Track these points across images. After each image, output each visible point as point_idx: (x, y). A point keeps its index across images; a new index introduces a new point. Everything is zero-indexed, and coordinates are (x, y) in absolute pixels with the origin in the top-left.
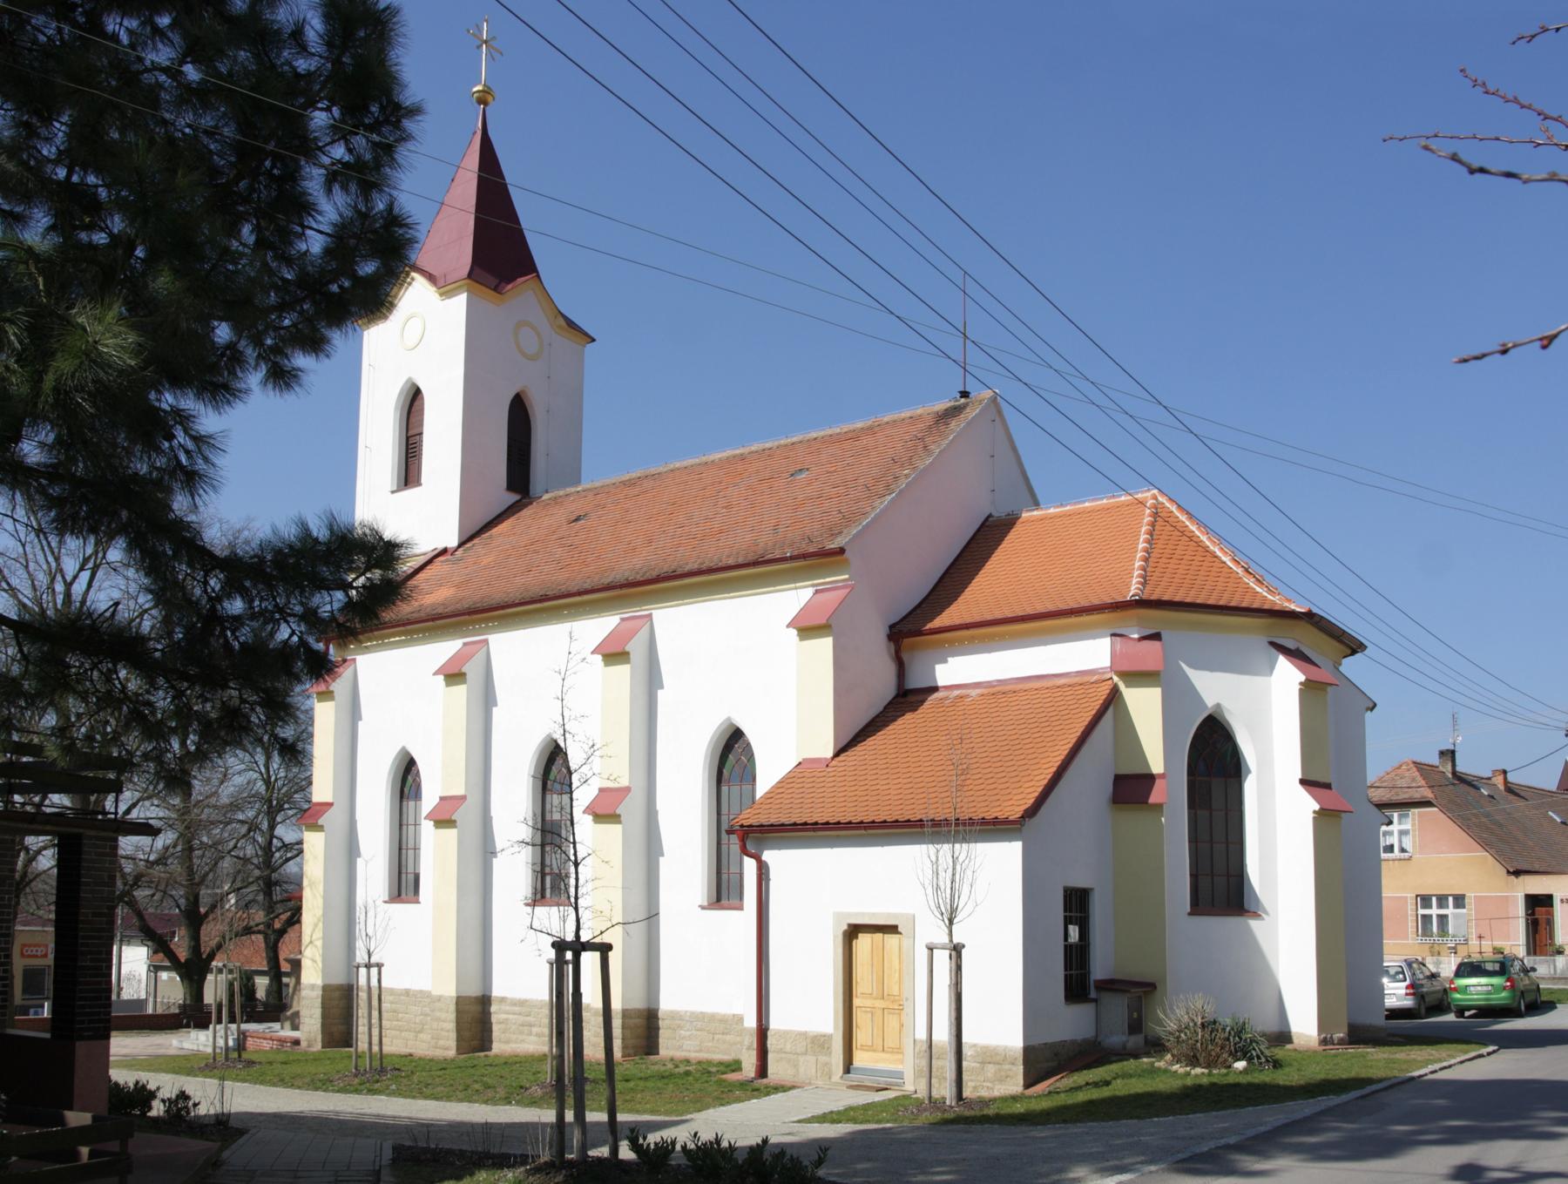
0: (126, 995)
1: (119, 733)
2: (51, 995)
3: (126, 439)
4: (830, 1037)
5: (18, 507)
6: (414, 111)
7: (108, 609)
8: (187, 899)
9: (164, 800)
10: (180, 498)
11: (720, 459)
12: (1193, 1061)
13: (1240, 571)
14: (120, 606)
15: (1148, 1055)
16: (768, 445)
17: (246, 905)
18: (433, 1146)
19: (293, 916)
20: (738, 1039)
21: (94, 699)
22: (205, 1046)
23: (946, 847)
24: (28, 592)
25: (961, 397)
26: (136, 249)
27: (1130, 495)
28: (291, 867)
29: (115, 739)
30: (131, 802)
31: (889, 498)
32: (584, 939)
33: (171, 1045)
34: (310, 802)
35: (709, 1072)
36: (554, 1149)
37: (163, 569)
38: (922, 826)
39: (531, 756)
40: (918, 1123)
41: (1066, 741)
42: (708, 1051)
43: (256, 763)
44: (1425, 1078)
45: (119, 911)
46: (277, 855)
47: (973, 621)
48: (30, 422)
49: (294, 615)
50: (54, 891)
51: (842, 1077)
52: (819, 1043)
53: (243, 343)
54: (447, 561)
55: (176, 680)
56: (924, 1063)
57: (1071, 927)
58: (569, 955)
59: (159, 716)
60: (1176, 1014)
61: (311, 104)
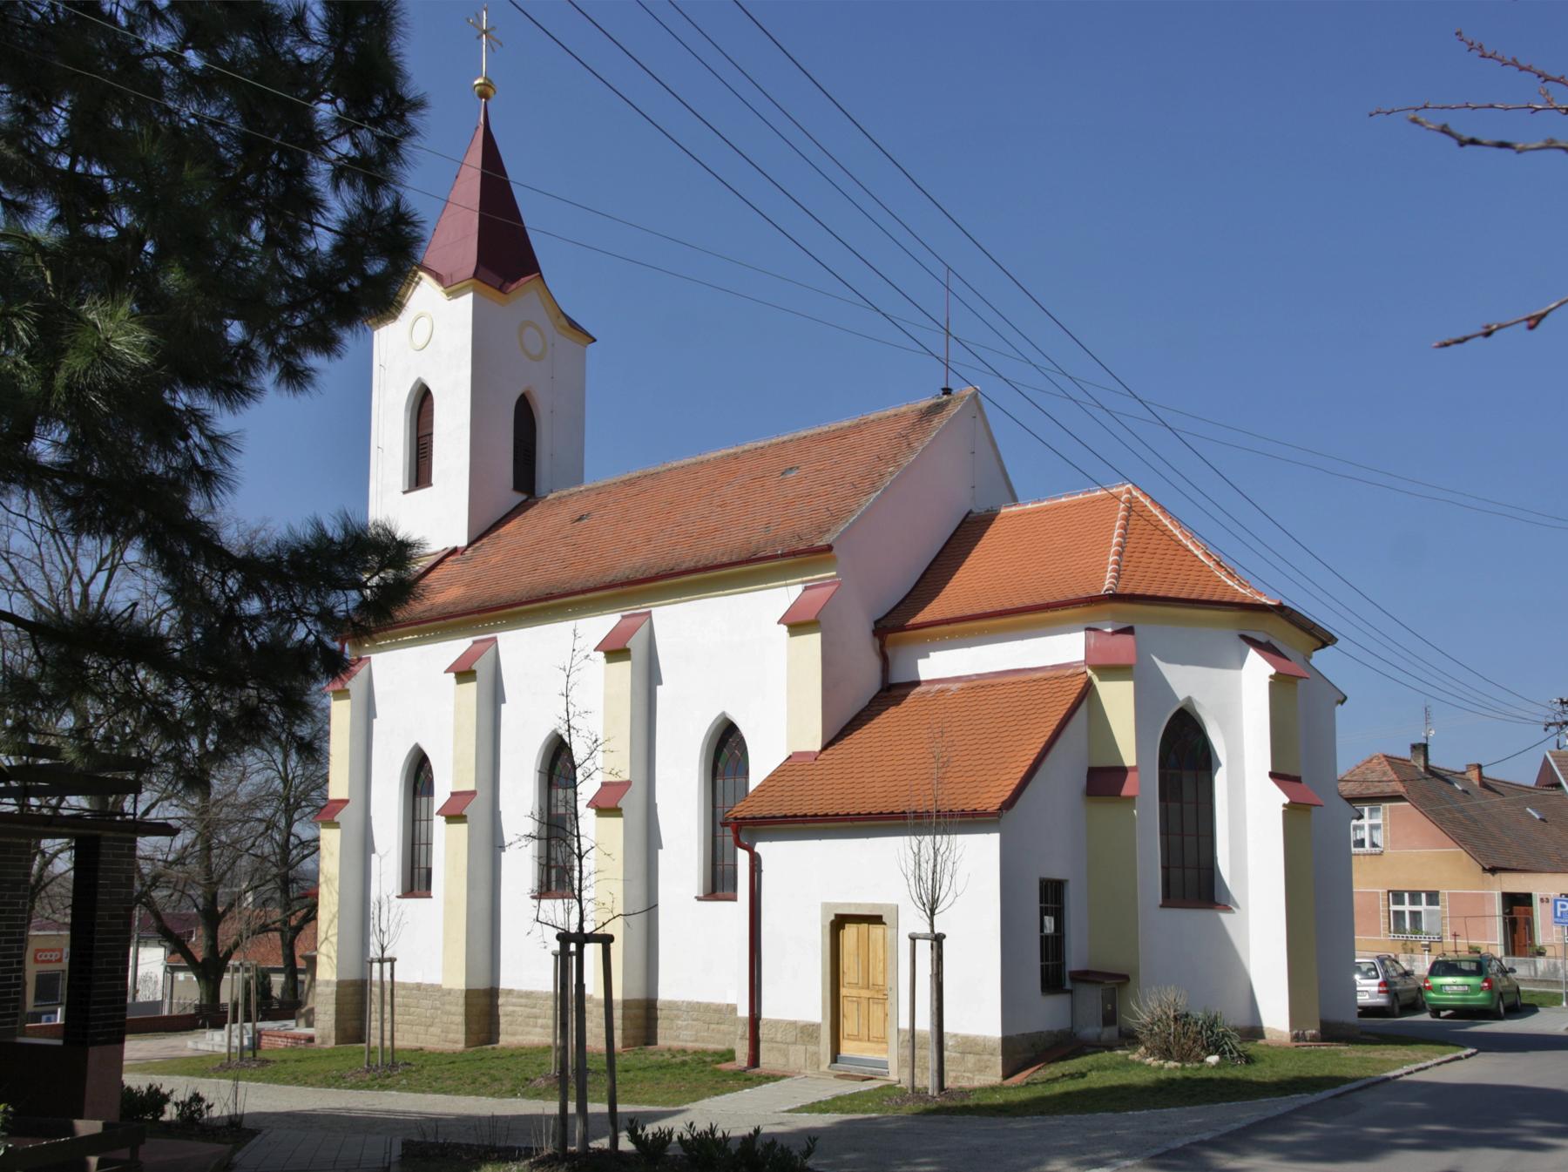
0: (142, 997)
1: (138, 734)
2: (65, 1001)
3: (141, 438)
4: (818, 1026)
5: (32, 507)
6: (418, 105)
7: (126, 610)
8: (205, 898)
9: (183, 800)
10: (197, 498)
11: (715, 458)
12: (1166, 1054)
13: (1212, 564)
14: (138, 607)
15: (1122, 1047)
16: (760, 444)
17: (263, 903)
18: (441, 1141)
19: (309, 913)
20: (732, 1029)
21: (113, 701)
22: (221, 1046)
23: (928, 839)
24: (44, 593)
25: (944, 394)
26: (144, 245)
27: (1105, 489)
28: (308, 864)
29: (134, 739)
30: (149, 803)
31: (874, 495)
32: (588, 928)
33: (186, 1046)
34: (326, 799)
35: (704, 1062)
36: (557, 1142)
37: (181, 569)
38: (905, 818)
39: (539, 747)
40: (902, 1113)
41: (1042, 734)
42: (703, 1041)
43: (274, 761)
44: (1401, 1079)
45: (136, 912)
46: (294, 852)
47: (952, 616)
48: (42, 421)
49: (311, 615)
50: (71, 895)
51: (829, 1067)
52: (807, 1032)
53: (256, 342)
54: (457, 560)
55: (195, 680)
56: (907, 1052)
57: (1047, 918)
58: (573, 947)
59: (179, 716)
60: (1148, 1006)
61: (316, 96)
